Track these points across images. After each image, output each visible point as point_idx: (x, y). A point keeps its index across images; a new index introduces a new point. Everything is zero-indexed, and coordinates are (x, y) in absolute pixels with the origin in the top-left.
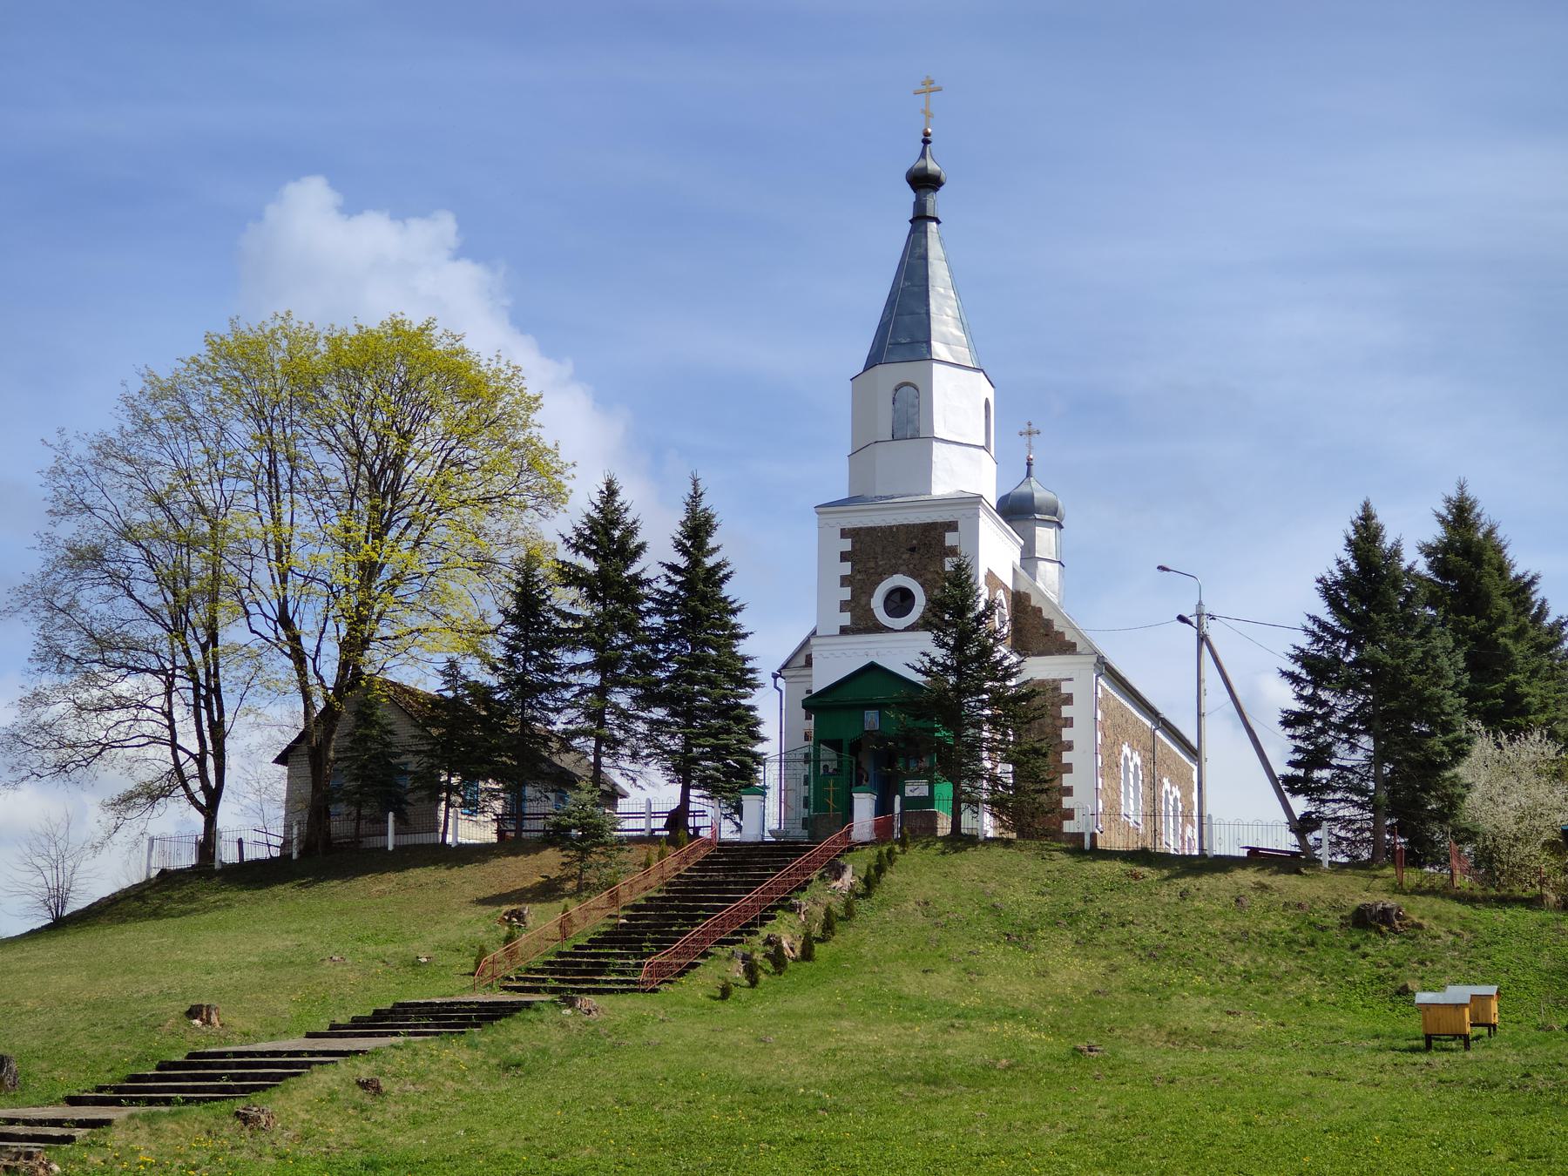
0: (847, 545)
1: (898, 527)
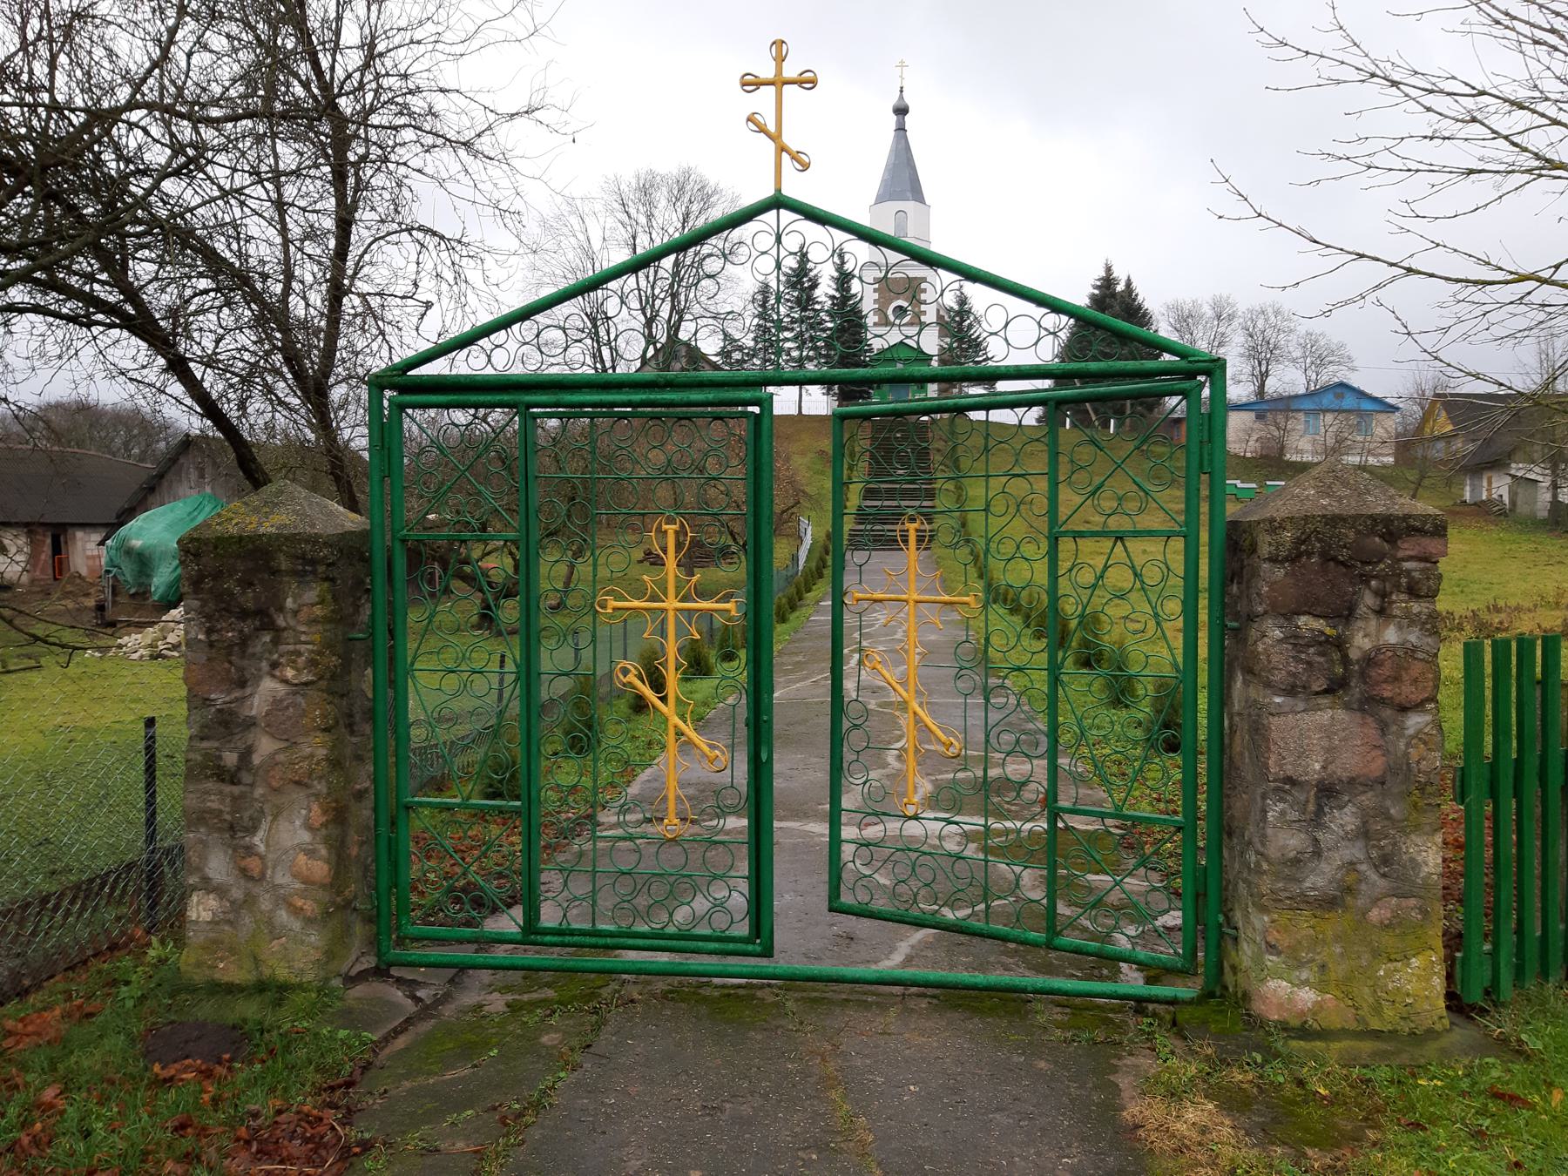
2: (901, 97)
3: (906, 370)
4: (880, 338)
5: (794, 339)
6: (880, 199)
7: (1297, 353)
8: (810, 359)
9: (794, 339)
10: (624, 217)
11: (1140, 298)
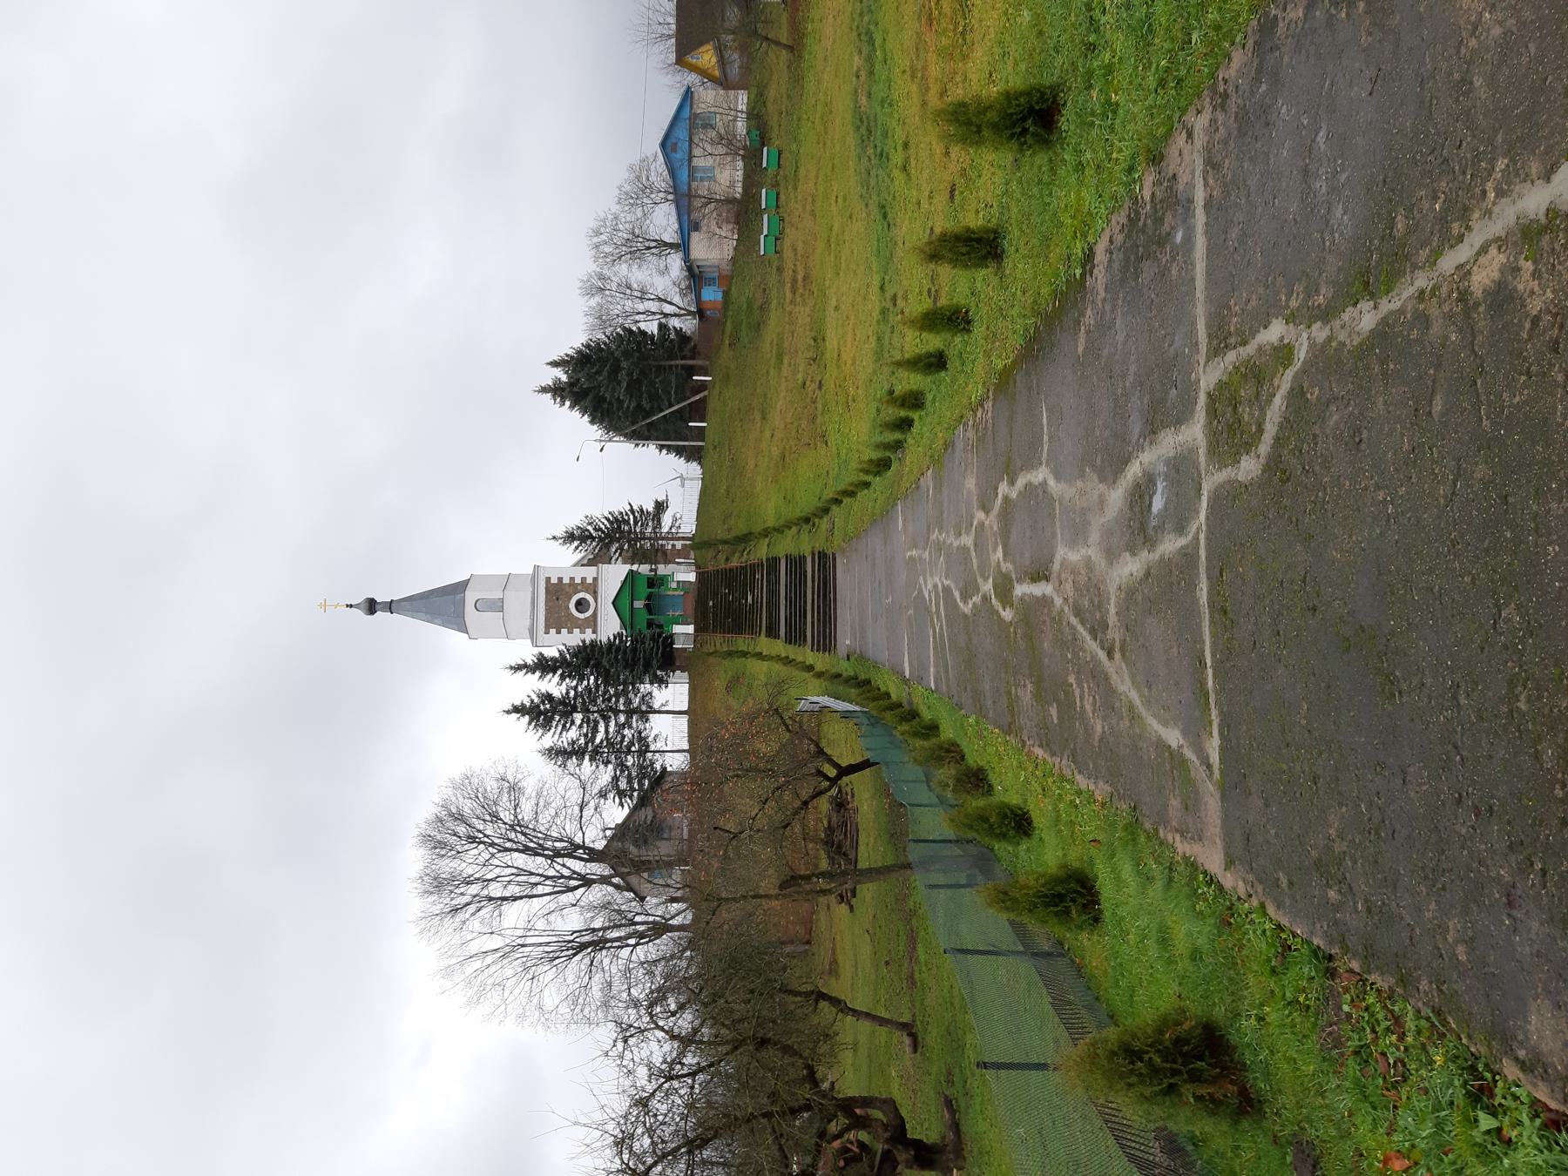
0: (553, 631)
2: (357, 606)
3: (644, 597)
4: (609, 626)
5: (606, 719)
6: (463, 629)
7: (639, 213)
8: (629, 702)
9: (606, 719)
10: (472, 908)
11: (570, 352)
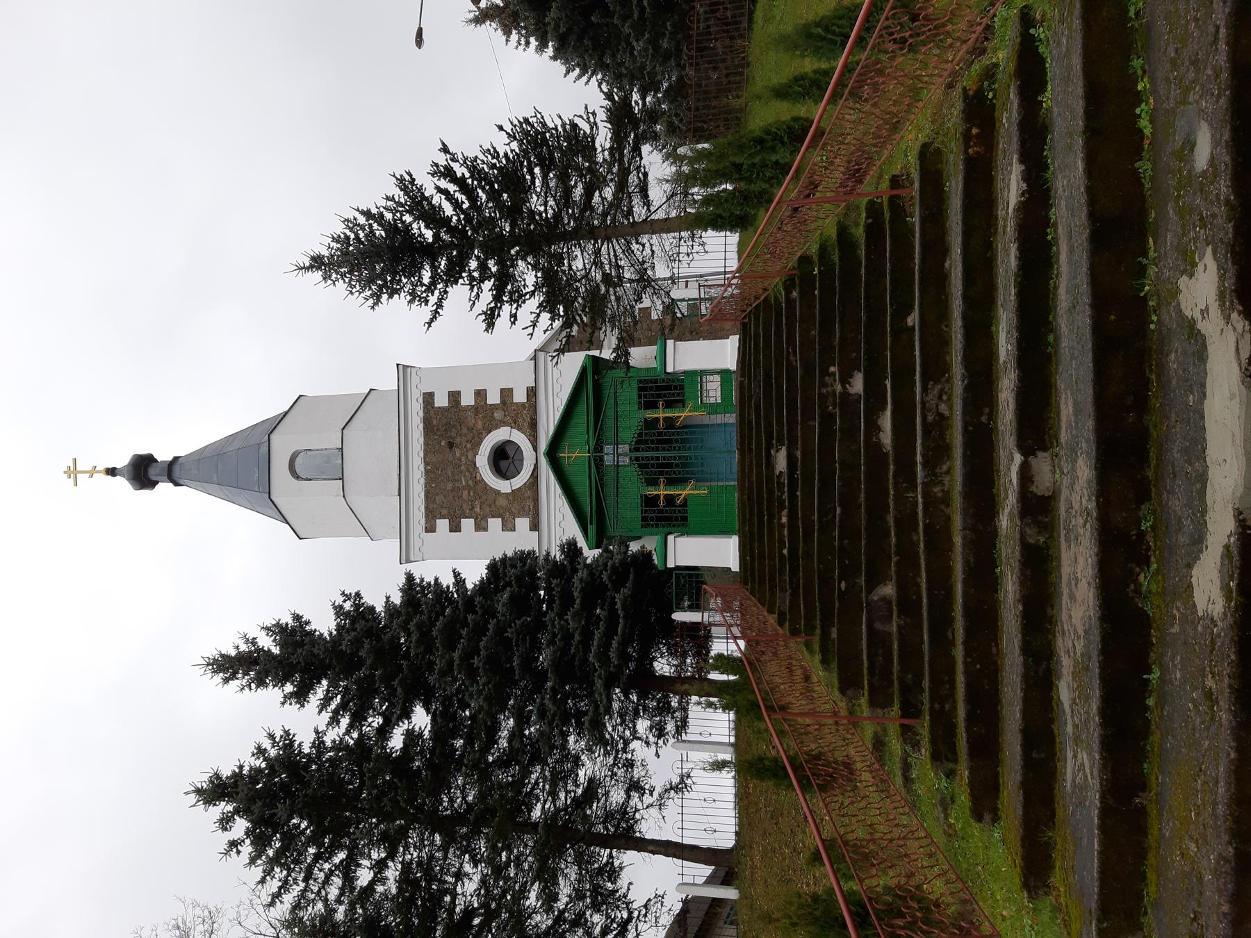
0: (443, 524)
1: (426, 464)
